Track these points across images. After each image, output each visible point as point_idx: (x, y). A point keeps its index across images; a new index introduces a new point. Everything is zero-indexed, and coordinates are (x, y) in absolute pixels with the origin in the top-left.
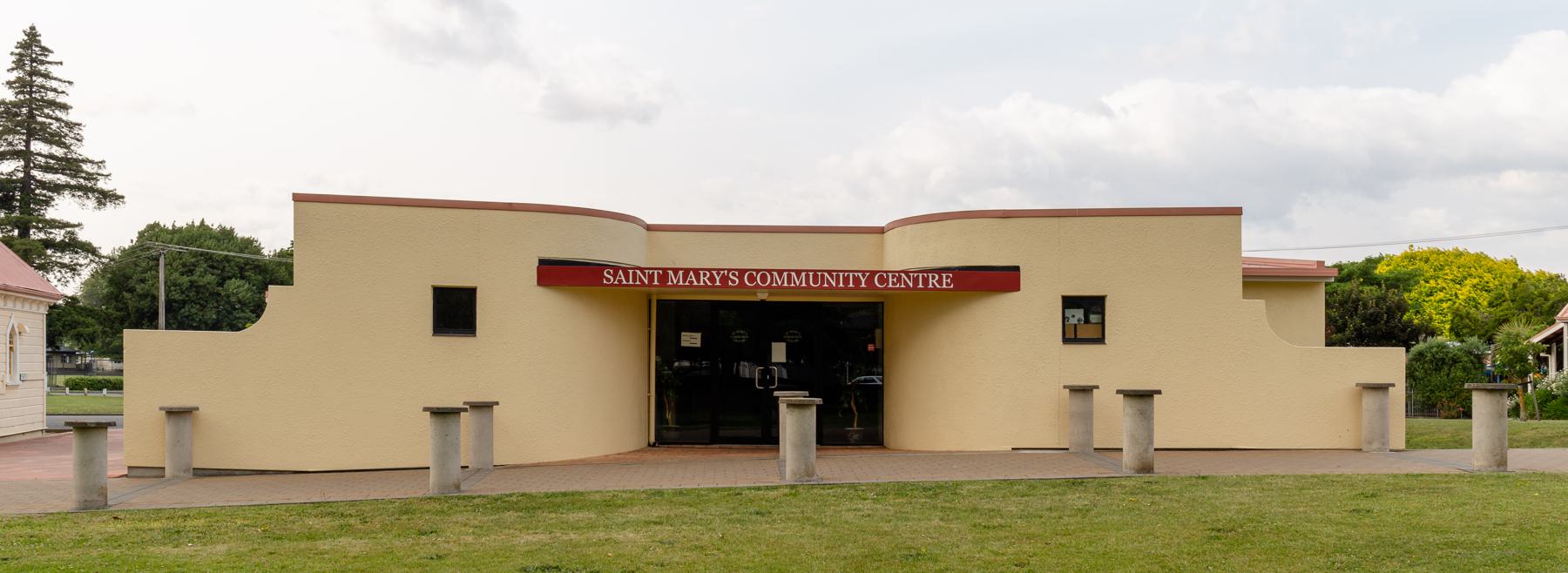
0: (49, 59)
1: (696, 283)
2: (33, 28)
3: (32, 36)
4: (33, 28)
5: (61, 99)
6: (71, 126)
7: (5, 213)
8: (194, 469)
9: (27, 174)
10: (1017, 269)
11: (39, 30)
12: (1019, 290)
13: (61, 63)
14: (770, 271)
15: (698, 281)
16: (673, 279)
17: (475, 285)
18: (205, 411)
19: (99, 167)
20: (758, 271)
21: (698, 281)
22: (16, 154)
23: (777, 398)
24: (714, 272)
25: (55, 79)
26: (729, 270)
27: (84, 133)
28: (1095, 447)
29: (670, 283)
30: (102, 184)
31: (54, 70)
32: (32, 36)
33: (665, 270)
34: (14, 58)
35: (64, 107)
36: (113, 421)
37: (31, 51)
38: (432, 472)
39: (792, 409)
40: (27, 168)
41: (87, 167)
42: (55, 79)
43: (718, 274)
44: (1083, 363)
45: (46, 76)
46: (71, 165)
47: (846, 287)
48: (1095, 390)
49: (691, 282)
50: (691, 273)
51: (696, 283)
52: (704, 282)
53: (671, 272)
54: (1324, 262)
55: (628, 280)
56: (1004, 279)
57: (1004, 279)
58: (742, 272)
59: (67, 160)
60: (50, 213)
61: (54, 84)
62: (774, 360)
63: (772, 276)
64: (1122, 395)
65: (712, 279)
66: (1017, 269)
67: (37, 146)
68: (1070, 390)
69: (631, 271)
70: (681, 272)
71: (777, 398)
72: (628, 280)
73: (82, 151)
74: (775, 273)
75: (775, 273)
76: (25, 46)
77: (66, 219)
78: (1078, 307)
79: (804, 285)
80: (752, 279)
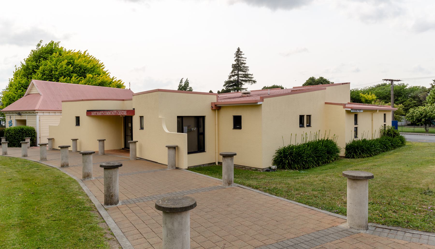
0: (242, 54)
2: (239, 48)
3: (239, 49)
4: (239, 48)
5: (244, 62)
6: (246, 67)
7: (398, 99)
8: (234, 164)
9: (238, 79)
11: (240, 48)
13: (244, 54)
18: (55, 138)
19: (252, 75)
22: (236, 75)
23: (1, 138)
25: (243, 58)
27: (249, 68)
30: (253, 79)
31: (242, 56)
32: (239, 49)
34: (235, 55)
35: (245, 64)
37: (238, 53)
39: (234, 153)
40: (238, 77)
41: (250, 76)
42: (243, 58)
45: (242, 58)
46: (246, 76)
59: (245, 75)
60: (243, 87)
61: (243, 59)
64: (82, 154)
67: (240, 73)
68: (168, 148)
71: (1, 138)
73: (249, 72)
76: (238, 52)
77: (244, 88)
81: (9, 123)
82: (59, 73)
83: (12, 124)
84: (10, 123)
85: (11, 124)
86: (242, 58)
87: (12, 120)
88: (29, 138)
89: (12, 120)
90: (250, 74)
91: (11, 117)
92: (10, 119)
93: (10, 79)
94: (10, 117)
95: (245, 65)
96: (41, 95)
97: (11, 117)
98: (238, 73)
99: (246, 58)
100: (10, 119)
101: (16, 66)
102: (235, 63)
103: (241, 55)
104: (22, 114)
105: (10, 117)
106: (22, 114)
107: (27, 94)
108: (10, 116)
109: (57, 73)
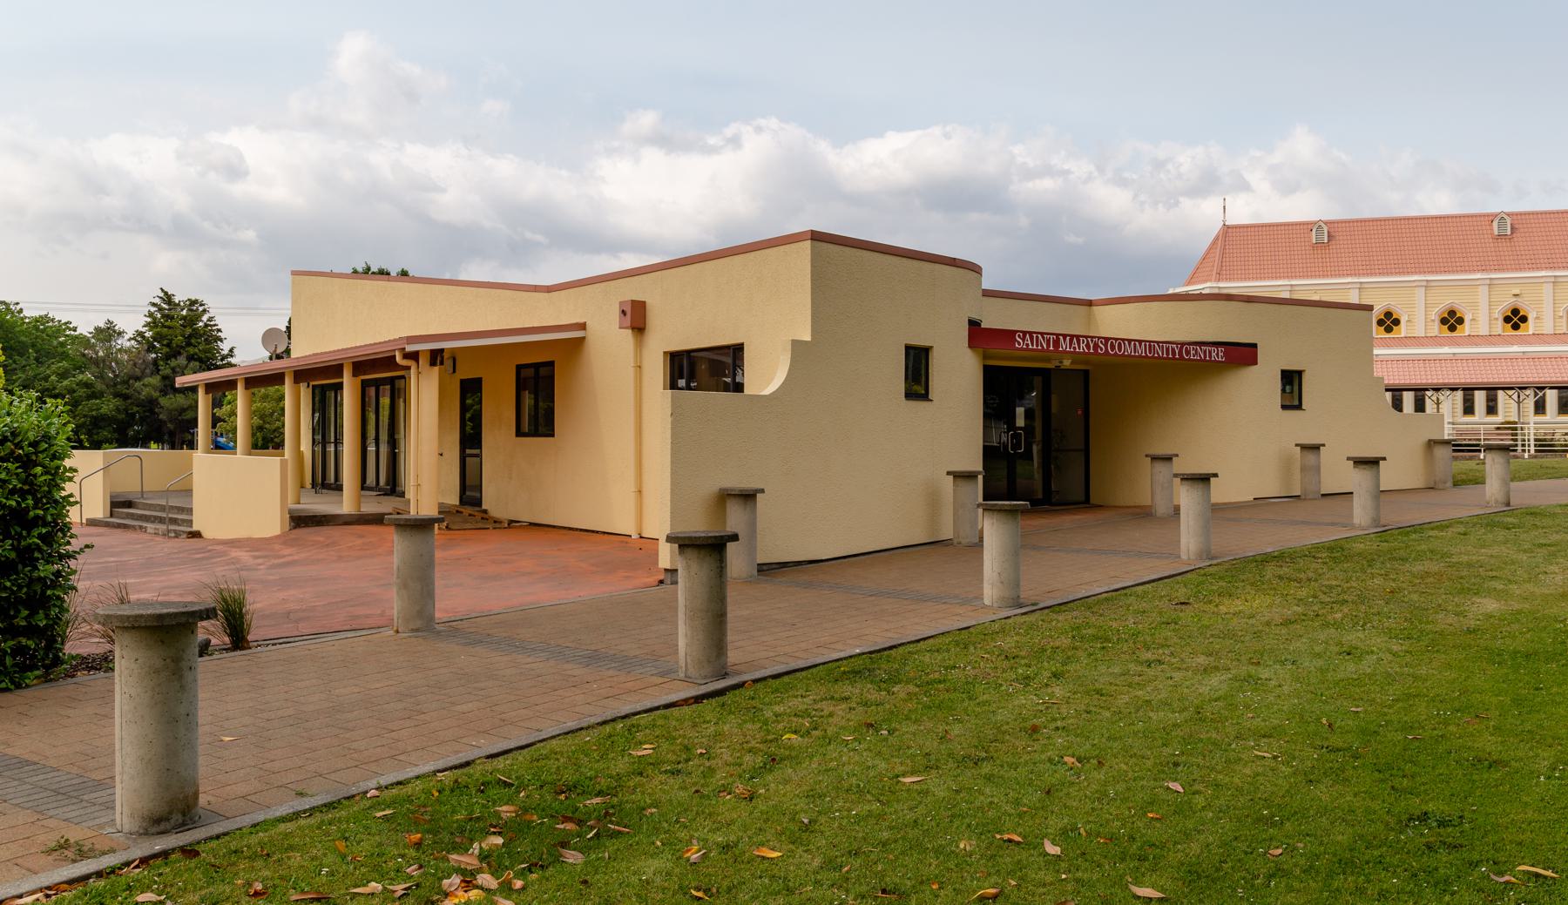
1: (1077, 350)
10: (1255, 346)
12: (1257, 364)
14: (1123, 340)
15: (1079, 349)
16: (1064, 345)
17: (739, 341)
20: (1116, 339)
21: (1079, 349)
24: (1089, 339)
26: (1099, 338)
28: (1322, 493)
29: (1061, 349)
33: (1057, 335)
36: (318, 498)
38: (1355, 497)
43: (1092, 341)
44: (1301, 427)
47: (1174, 358)
48: (1321, 448)
49: (1075, 348)
50: (1028, 336)
51: (1077, 350)
52: (1083, 349)
53: (1061, 338)
54: (796, 344)
55: (1033, 345)
56: (1242, 354)
57: (1242, 354)
58: (1107, 339)
62: (1018, 425)
63: (1124, 344)
65: (1088, 346)
66: (1255, 346)
69: (1035, 335)
70: (1068, 338)
72: (1033, 345)
74: (1126, 342)
75: (1126, 342)
78: (325, 394)
79: (1144, 354)
80: (1113, 347)
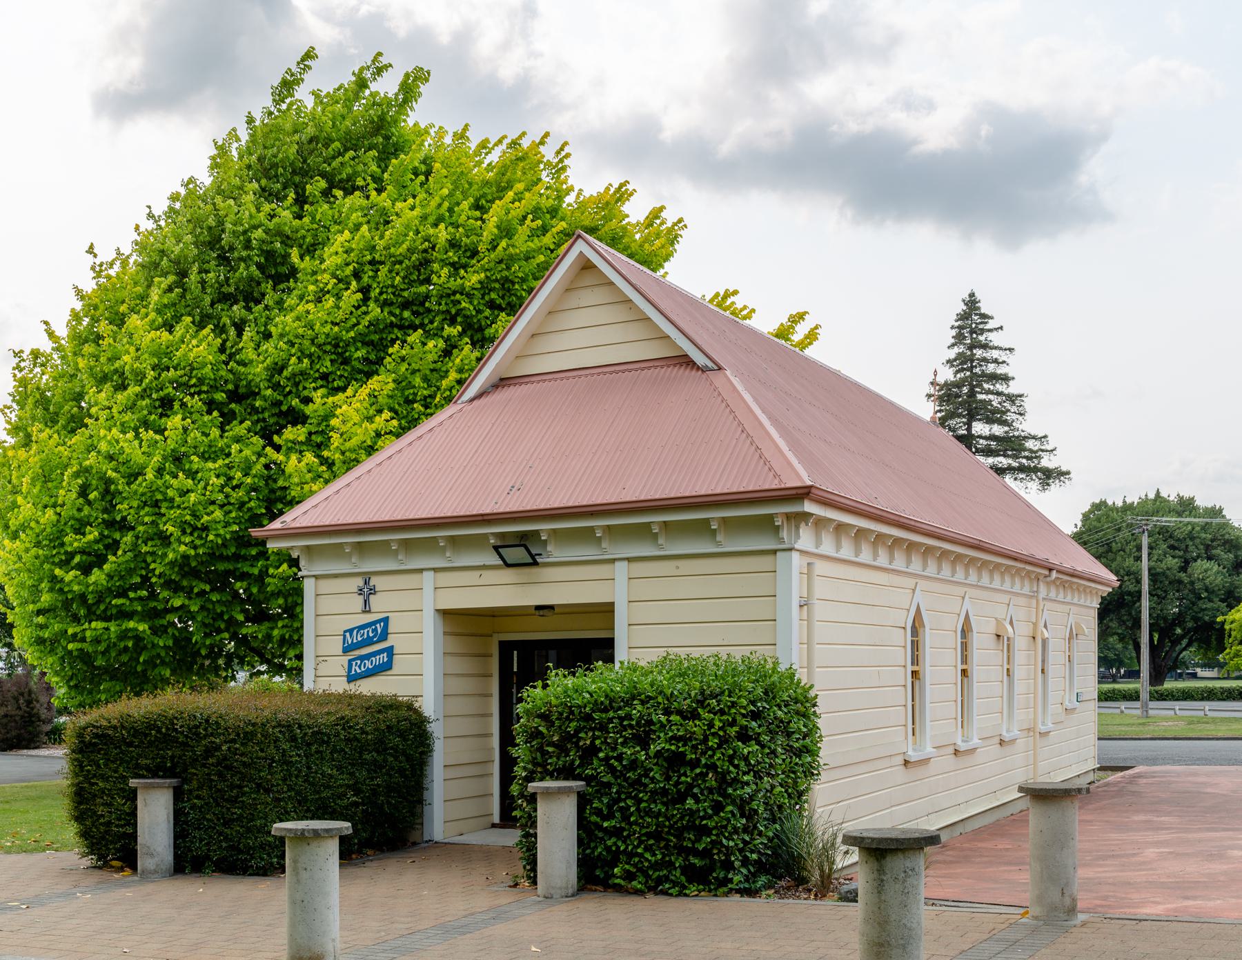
0: (988, 327)
2: (972, 295)
3: (972, 303)
4: (972, 295)
5: (1001, 370)
6: (1012, 398)
11: (978, 296)
13: (1001, 328)
25: (996, 348)
30: (1047, 462)
31: (995, 338)
32: (972, 303)
35: (1006, 379)
42: (996, 348)
45: (985, 346)
61: (995, 354)
73: (1026, 426)
81: (346, 650)
82: (485, 287)
83: (390, 651)
84: (368, 642)
85: (384, 657)
86: (985, 346)
87: (386, 620)
88: (561, 791)
89: (386, 620)
90: (1034, 438)
91: (373, 591)
92: (367, 610)
93: (24, 356)
94: (367, 592)
95: (1013, 389)
96: (704, 370)
97: (373, 591)
98: (969, 429)
99: (1011, 350)
100: (367, 610)
101: (92, 247)
102: (947, 375)
103: (982, 331)
104: (555, 552)
105: (367, 592)
106: (555, 552)
107: (495, 379)
108: (367, 578)
109: (473, 279)
